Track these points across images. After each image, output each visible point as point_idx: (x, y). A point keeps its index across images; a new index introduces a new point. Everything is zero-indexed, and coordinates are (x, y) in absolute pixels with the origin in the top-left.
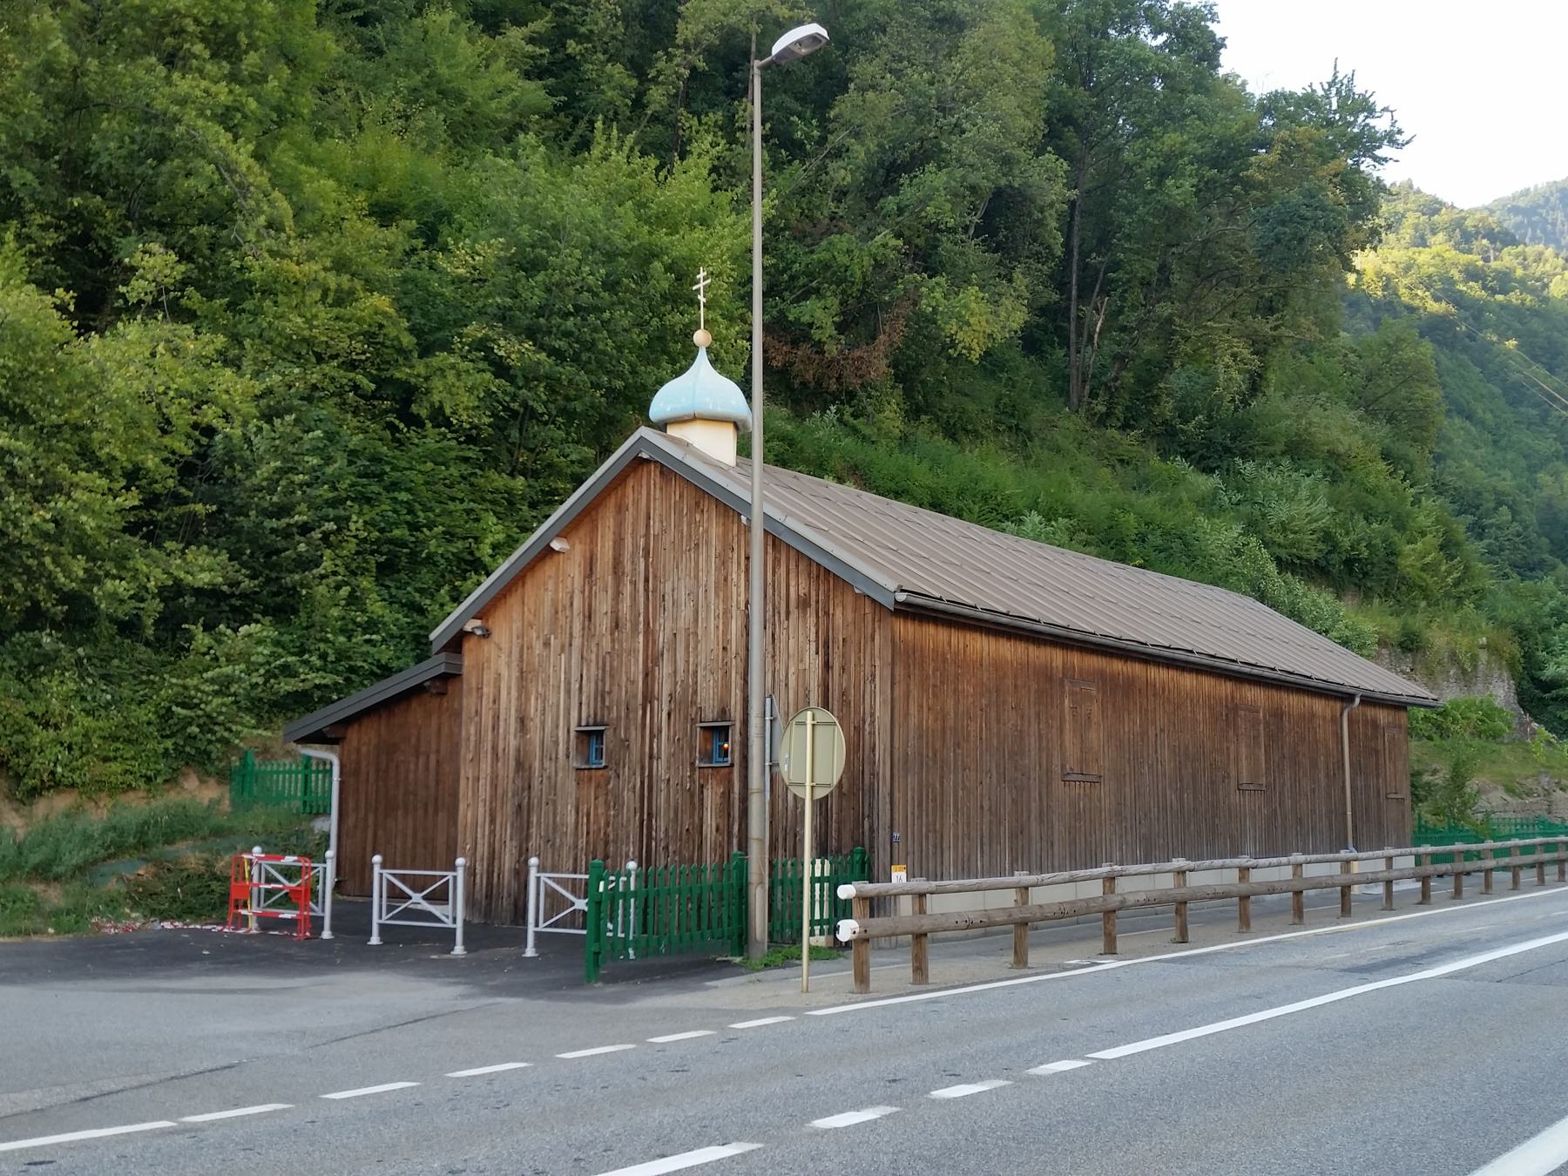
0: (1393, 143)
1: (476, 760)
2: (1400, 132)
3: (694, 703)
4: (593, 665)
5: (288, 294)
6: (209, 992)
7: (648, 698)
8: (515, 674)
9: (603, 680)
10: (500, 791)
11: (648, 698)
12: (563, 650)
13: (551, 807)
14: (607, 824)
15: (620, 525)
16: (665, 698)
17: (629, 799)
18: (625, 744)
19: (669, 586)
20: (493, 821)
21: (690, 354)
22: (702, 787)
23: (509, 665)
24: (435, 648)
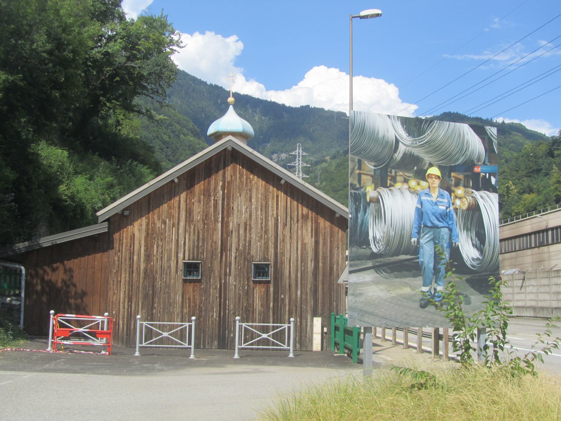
0: (178, 46)
1: (119, 272)
2: (181, 42)
3: (249, 253)
4: (192, 234)
5: (118, 54)
6: (220, 374)
7: (224, 248)
8: (144, 235)
9: (198, 241)
10: (134, 287)
11: (224, 248)
12: (173, 226)
13: (166, 295)
14: (201, 303)
15: (224, 173)
16: (234, 250)
17: (214, 293)
18: (211, 270)
19: (236, 203)
20: (130, 300)
21: (227, 106)
22: (254, 288)
23: (140, 230)
24: (100, 220)
